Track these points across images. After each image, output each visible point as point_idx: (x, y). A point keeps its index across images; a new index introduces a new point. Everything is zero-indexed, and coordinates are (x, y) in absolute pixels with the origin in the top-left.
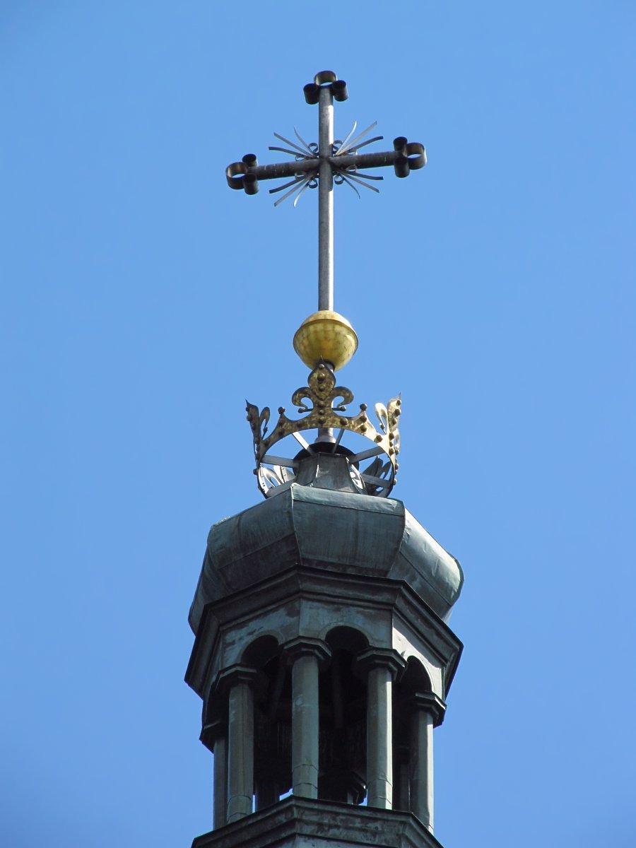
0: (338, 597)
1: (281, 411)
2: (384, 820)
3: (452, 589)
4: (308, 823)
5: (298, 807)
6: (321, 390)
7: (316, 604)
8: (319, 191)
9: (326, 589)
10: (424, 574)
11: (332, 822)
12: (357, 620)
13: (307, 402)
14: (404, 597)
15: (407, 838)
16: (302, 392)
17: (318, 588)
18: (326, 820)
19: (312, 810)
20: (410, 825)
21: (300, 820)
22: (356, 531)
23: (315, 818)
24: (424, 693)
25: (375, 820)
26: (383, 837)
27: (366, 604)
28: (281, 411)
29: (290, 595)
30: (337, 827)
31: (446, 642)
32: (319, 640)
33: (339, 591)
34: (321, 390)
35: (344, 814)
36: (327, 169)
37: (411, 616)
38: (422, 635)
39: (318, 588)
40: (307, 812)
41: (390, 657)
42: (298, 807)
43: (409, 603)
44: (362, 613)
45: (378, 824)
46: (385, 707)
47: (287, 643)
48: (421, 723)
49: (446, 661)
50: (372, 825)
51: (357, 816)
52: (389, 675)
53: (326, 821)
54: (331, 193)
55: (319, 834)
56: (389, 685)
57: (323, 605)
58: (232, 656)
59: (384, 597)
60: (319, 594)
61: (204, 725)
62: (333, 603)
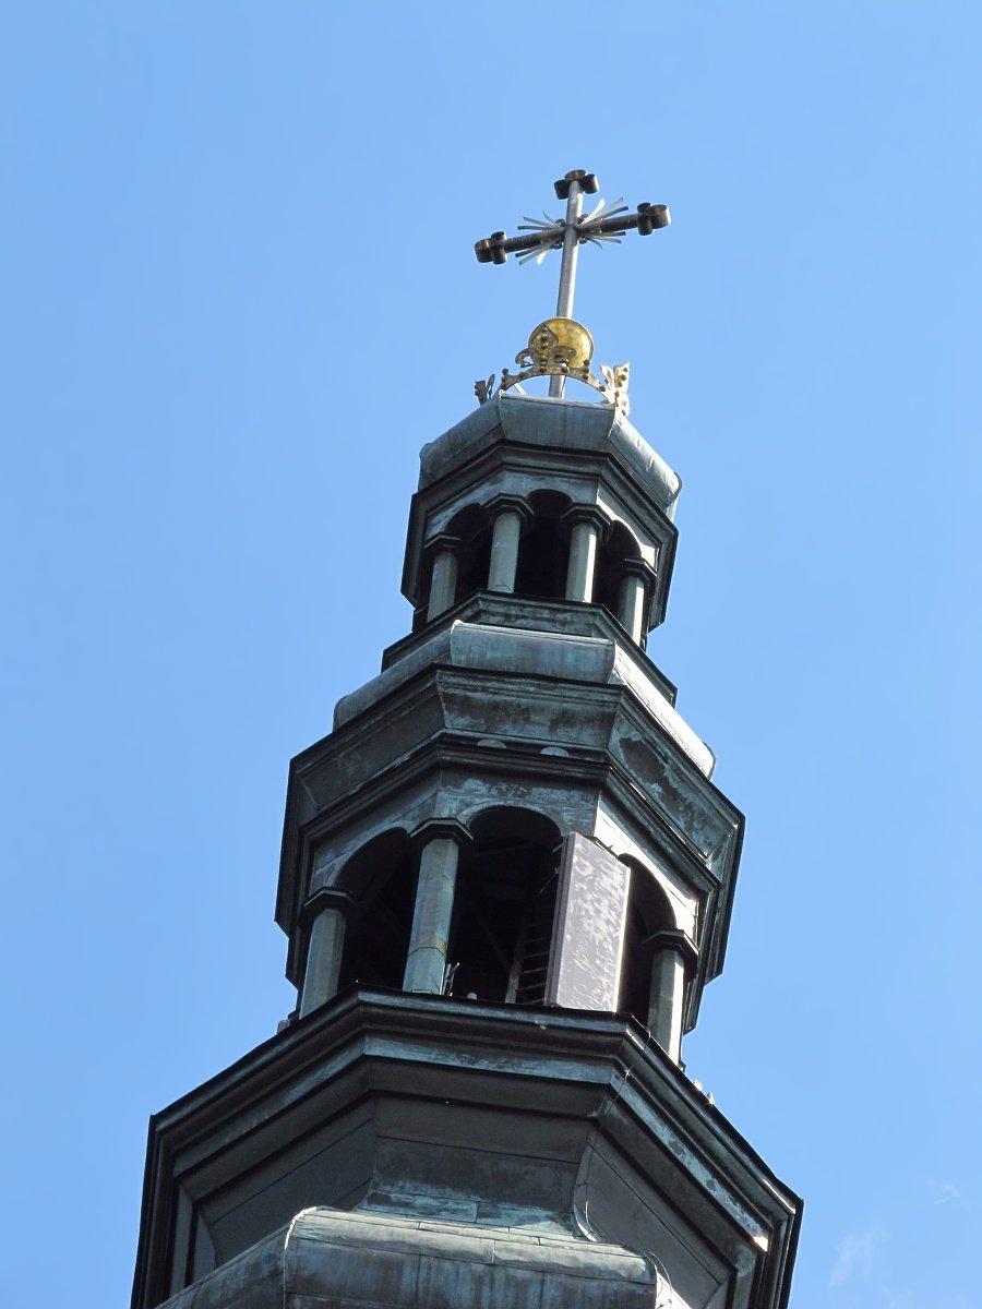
0: (542, 468)
1: (505, 372)
2: (574, 611)
3: (669, 490)
4: (494, 614)
5: (484, 600)
6: (544, 348)
7: (519, 475)
8: (564, 255)
9: (531, 462)
10: (638, 468)
11: (519, 613)
12: (561, 485)
13: (528, 359)
14: (611, 470)
15: (597, 627)
16: (526, 352)
17: (522, 461)
18: (513, 612)
19: (499, 602)
20: (600, 615)
21: (486, 612)
22: (564, 420)
23: (502, 609)
24: (633, 558)
25: (565, 611)
26: (572, 627)
27: (572, 475)
28: (505, 372)
29: (496, 468)
30: (523, 617)
31: (661, 526)
32: (521, 497)
33: (542, 464)
34: (544, 348)
35: (531, 606)
36: (570, 235)
37: (616, 487)
38: (637, 517)
39: (522, 461)
40: (493, 605)
41: (592, 516)
42: (484, 600)
43: (615, 476)
44: (568, 482)
45: (568, 616)
46: (586, 560)
47: (488, 503)
48: (630, 585)
49: (661, 543)
50: (560, 616)
51: (546, 608)
52: (592, 529)
53: (513, 612)
54: (576, 249)
55: (506, 624)
56: (593, 539)
57: (527, 475)
58: (439, 524)
59: (591, 469)
60: (524, 466)
61: (546, 972)
62: (538, 474)
